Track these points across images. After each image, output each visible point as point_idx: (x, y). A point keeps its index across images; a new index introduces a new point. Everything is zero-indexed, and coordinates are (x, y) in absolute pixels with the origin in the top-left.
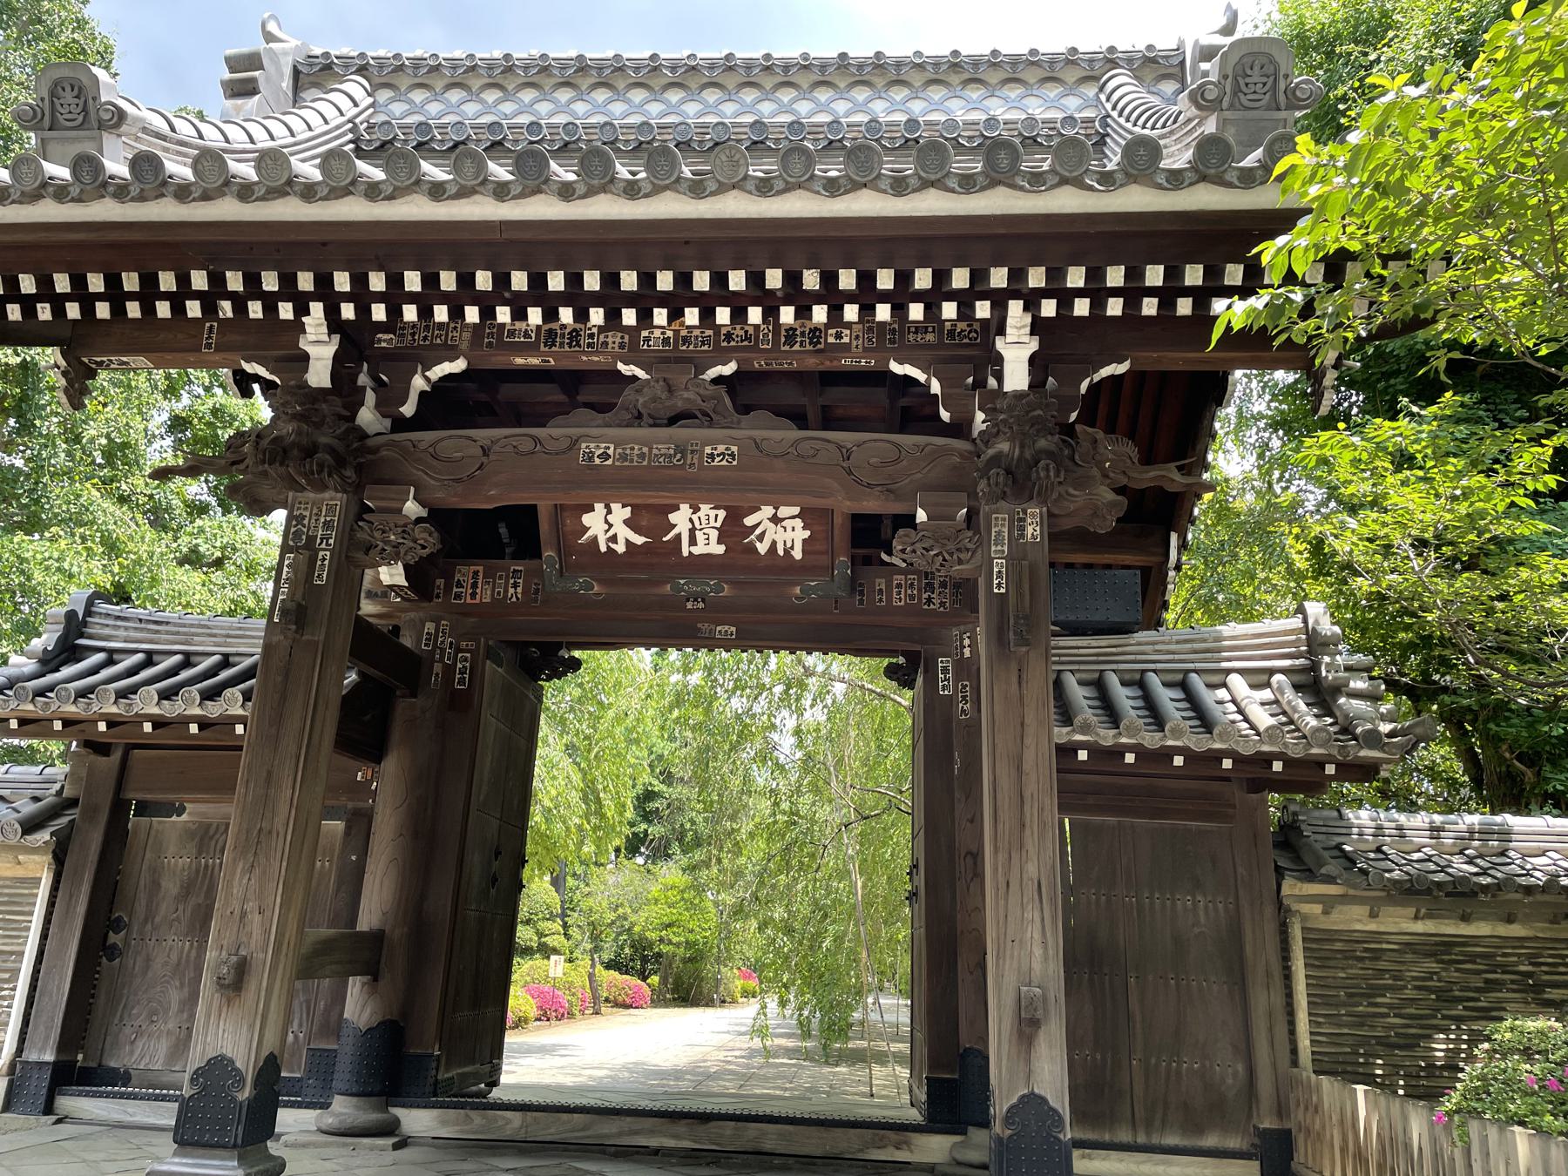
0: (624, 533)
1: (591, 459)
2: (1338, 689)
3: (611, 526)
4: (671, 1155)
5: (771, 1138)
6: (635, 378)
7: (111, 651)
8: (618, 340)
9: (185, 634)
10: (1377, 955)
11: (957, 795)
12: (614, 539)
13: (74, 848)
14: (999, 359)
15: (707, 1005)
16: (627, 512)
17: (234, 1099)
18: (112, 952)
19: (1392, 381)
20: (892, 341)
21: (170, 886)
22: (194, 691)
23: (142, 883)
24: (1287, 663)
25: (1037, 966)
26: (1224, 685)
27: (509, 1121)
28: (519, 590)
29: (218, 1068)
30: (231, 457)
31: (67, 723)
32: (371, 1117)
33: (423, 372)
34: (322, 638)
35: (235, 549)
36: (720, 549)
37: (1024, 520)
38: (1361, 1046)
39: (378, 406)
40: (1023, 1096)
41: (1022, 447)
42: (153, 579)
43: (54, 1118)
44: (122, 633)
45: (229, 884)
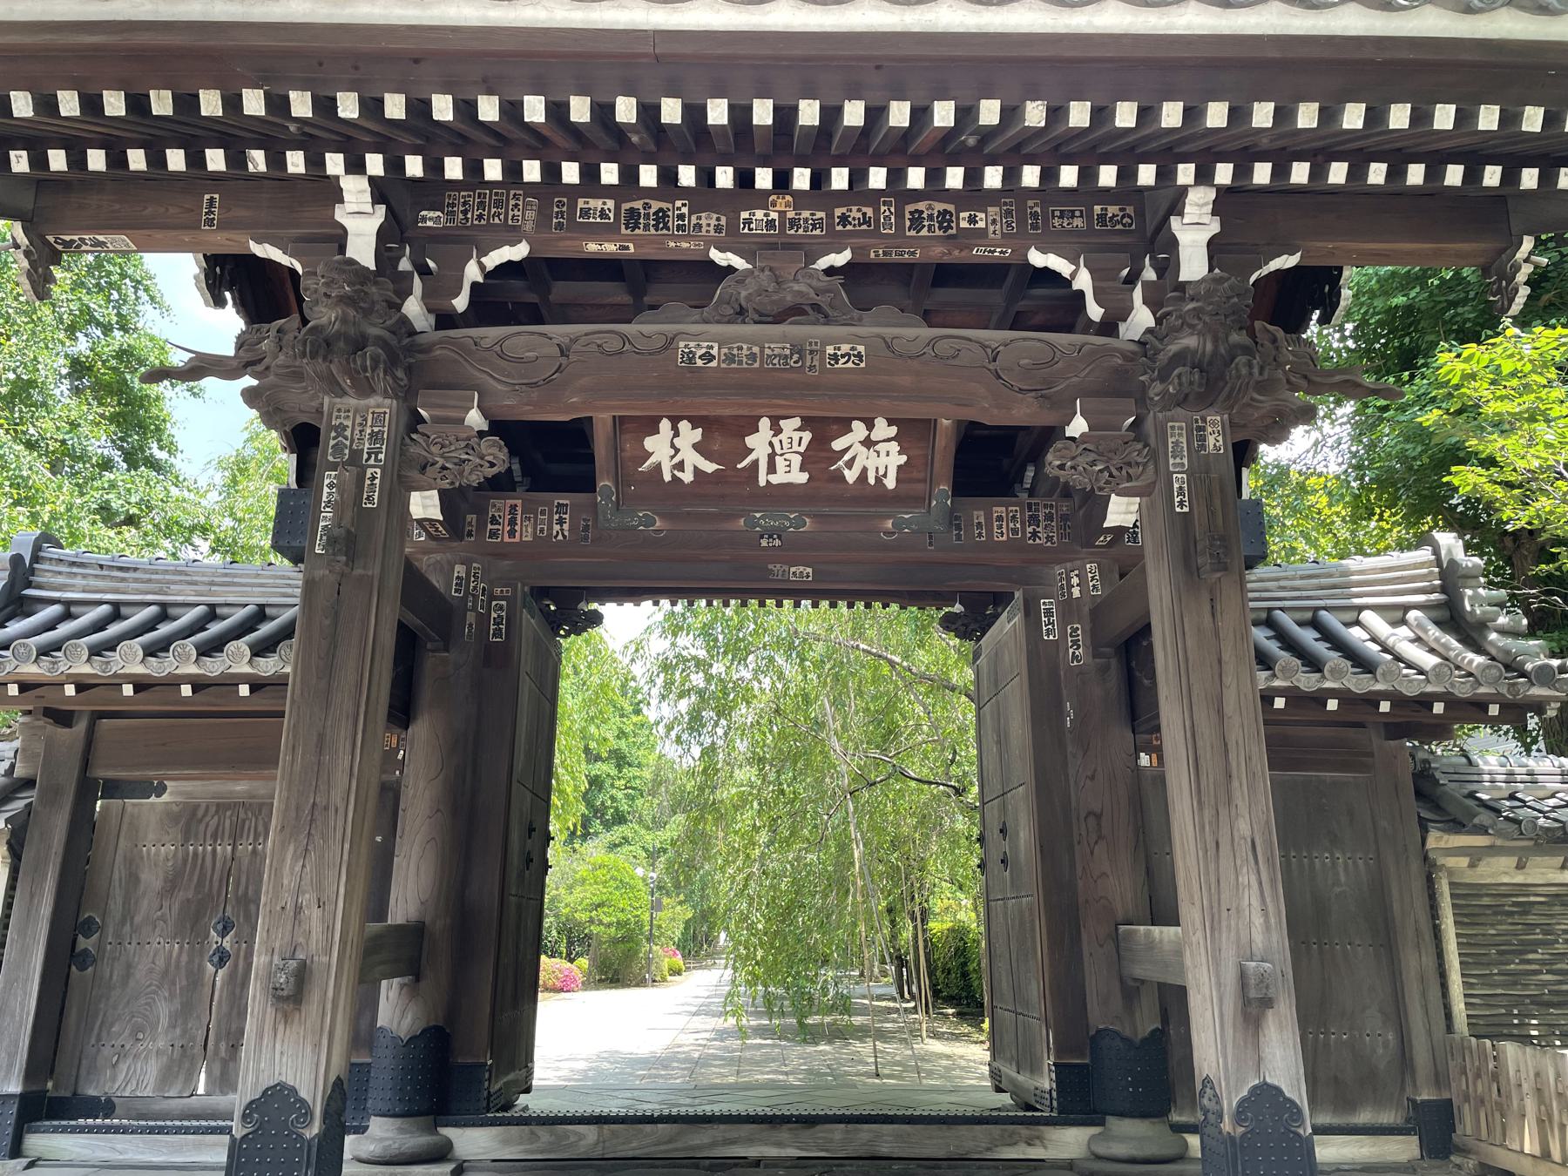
0: (693, 459)
1: (691, 360)
2: (1483, 625)
3: (677, 451)
4: (775, 1166)
5: (887, 1141)
6: (730, 269)
7: (68, 604)
8: (713, 222)
9: (158, 582)
10: (1526, 908)
11: (1070, 749)
12: (680, 466)
13: (33, 835)
14: (1173, 243)
15: (637, 985)
16: (697, 435)
17: (300, 1136)
18: (84, 960)
19: (1460, 310)
20: (1035, 227)
21: (152, 879)
22: (189, 645)
23: (116, 876)
24: (1421, 598)
25: (1258, 938)
26: (1358, 623)
27: (581, 1137)
28: (566, 527)
29: (277, 1102)
30: (246, 356)
31: (24, 687)
32: (418, 1141)
33: (479, 257)
34: (377, 571)
35: (150, 508)
36: (803, 478)
37: (1203, 429)
38: (1515, 1006)
39: (426, 297)
40: (1255, 1088)
41: (1215, 341)
42: (72, 534)
43: (24, 1161)
44: (78, 581)
45: (277, 873)
